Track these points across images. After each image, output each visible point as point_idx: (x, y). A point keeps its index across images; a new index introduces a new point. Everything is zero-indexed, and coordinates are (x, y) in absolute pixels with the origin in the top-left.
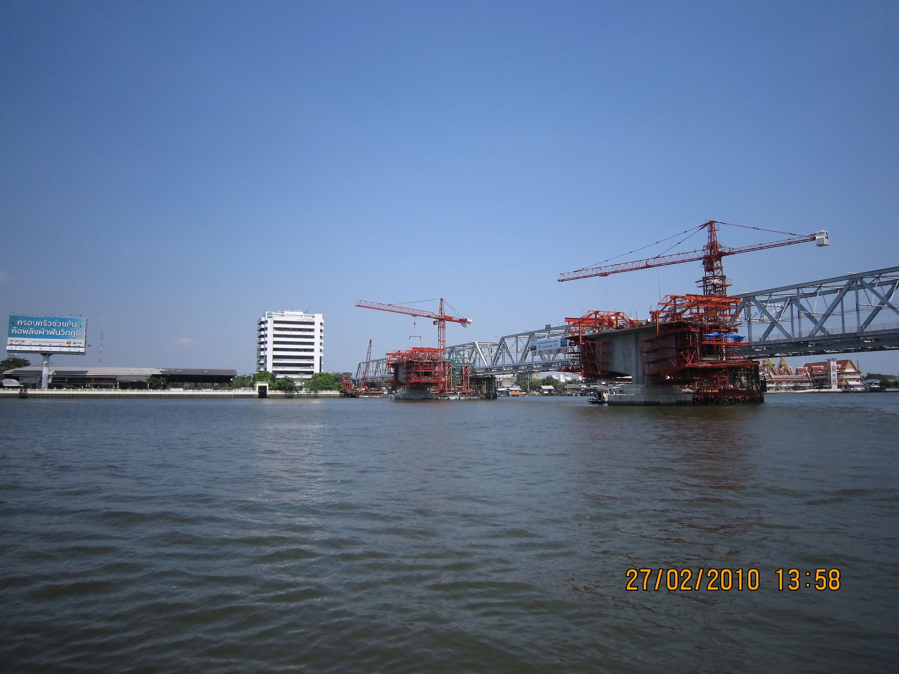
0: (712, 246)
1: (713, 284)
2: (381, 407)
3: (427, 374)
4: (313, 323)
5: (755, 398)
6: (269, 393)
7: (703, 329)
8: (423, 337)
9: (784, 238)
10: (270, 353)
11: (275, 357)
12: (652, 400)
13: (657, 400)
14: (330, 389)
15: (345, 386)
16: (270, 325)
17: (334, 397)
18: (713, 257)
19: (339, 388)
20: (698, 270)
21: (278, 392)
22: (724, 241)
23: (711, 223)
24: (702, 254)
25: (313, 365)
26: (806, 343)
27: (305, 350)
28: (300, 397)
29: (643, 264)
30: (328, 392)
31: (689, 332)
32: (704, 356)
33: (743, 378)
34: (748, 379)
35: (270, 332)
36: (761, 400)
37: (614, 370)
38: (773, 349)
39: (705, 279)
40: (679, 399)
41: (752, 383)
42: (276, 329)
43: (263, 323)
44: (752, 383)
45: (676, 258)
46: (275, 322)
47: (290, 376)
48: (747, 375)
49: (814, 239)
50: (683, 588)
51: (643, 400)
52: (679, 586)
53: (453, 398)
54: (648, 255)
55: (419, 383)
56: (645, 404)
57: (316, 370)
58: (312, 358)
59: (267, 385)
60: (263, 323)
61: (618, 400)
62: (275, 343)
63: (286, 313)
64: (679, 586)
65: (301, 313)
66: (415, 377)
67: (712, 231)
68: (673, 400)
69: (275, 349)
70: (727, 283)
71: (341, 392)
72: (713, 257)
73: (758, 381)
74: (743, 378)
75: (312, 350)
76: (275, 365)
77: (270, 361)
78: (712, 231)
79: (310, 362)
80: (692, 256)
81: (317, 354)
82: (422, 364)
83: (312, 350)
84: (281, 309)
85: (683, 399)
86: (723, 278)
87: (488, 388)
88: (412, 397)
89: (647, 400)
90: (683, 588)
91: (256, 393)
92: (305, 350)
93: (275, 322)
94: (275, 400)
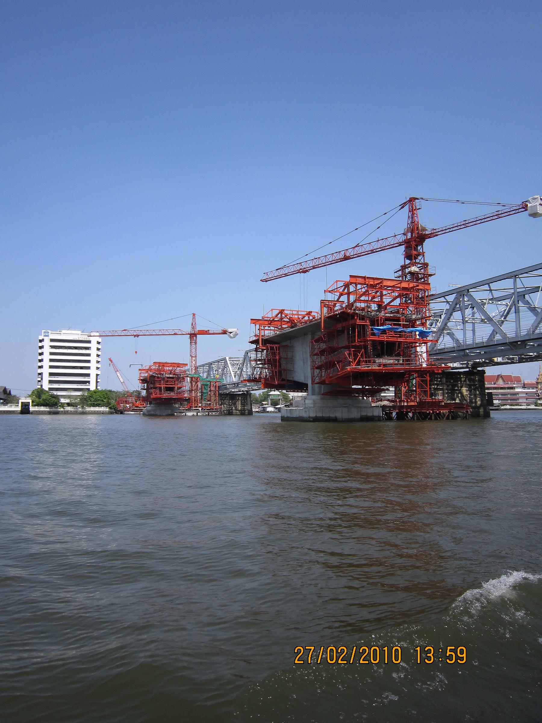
0: (413, 227)
1: (410, 273)
2: (132, 421)
3: (171, 389)
4: (89, 342)
5: (481, 410)
6: (32, 409)
7: (374, 322)
8: (174, 352)
9: (491, 210)
10: (46, 371)
11: (51, 374)
12: (326, 415)
13: (332, 415)
14: (98, 405)
15: (111, 402)
16: (47, 343)
17: (103, 413)
18: (415, 241)
19: (107, 405)
20: (397, 257)
21: (42, 409)
22: (427, 220)
23: (412, 200)
24: (401, 238)
25: (89, 382)
26: (524, 342)
27: (82, 368)
28: (66, 413)
29: (341, 256)
30: (97, 409)
31: (354, 327)
32: (379, 356)
33: (465, 390)
34: (470, 391)
35: (47, 350)
36: (487, 415)
37: (296, 379)
38: (491, 351)
39: (404, 267)
40: (364, 414)
41: (475, 395)
42: (52, 347)
43: (41, 341)
44: (475, 395)
45: (375, 246)
46: (52, 340)
47: (55, 393)
48: (469, 386)
49: (525, 208)
50: (340, 662)
51: (313, 415)
52: (337, 660)
53: (189, 414)
54: (345, 245)
55: (160, 399)
56: (316, 420)
57: (92, 387)
58: (88, 375)
59: (30, 401)
60: (41, 341)
61: (289, 415)
62: (51, 360)
63: (64, 331)
64: (337, 660)
65: (79, 332)
66: (163, 393)
67: (412, 211)
68: (355, 414)
69: (51, 367)
70: (430, 272)
71: (110, 408)
72: (415, 241)
73: (482, 394)
74: (465, 390)
75: (88, 368)
76: (51, 382)
77: (46, 378)
78: (412, 211)
79: (86, 379)
80: (392, 241)
81: (93, 372)
82: (164, 379)
83: (88, 368)
84: (57, 329)
85: (370, 414)
86: (425, 265)
87: (243, 405)
88: (158, 413)
89: (319, 415)
90: (340, 662)
91: (19, 409)
92: (82, 368)
93: (52, 340)
94: (45, 419)
